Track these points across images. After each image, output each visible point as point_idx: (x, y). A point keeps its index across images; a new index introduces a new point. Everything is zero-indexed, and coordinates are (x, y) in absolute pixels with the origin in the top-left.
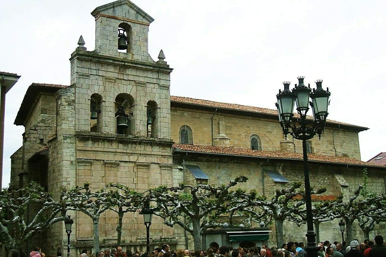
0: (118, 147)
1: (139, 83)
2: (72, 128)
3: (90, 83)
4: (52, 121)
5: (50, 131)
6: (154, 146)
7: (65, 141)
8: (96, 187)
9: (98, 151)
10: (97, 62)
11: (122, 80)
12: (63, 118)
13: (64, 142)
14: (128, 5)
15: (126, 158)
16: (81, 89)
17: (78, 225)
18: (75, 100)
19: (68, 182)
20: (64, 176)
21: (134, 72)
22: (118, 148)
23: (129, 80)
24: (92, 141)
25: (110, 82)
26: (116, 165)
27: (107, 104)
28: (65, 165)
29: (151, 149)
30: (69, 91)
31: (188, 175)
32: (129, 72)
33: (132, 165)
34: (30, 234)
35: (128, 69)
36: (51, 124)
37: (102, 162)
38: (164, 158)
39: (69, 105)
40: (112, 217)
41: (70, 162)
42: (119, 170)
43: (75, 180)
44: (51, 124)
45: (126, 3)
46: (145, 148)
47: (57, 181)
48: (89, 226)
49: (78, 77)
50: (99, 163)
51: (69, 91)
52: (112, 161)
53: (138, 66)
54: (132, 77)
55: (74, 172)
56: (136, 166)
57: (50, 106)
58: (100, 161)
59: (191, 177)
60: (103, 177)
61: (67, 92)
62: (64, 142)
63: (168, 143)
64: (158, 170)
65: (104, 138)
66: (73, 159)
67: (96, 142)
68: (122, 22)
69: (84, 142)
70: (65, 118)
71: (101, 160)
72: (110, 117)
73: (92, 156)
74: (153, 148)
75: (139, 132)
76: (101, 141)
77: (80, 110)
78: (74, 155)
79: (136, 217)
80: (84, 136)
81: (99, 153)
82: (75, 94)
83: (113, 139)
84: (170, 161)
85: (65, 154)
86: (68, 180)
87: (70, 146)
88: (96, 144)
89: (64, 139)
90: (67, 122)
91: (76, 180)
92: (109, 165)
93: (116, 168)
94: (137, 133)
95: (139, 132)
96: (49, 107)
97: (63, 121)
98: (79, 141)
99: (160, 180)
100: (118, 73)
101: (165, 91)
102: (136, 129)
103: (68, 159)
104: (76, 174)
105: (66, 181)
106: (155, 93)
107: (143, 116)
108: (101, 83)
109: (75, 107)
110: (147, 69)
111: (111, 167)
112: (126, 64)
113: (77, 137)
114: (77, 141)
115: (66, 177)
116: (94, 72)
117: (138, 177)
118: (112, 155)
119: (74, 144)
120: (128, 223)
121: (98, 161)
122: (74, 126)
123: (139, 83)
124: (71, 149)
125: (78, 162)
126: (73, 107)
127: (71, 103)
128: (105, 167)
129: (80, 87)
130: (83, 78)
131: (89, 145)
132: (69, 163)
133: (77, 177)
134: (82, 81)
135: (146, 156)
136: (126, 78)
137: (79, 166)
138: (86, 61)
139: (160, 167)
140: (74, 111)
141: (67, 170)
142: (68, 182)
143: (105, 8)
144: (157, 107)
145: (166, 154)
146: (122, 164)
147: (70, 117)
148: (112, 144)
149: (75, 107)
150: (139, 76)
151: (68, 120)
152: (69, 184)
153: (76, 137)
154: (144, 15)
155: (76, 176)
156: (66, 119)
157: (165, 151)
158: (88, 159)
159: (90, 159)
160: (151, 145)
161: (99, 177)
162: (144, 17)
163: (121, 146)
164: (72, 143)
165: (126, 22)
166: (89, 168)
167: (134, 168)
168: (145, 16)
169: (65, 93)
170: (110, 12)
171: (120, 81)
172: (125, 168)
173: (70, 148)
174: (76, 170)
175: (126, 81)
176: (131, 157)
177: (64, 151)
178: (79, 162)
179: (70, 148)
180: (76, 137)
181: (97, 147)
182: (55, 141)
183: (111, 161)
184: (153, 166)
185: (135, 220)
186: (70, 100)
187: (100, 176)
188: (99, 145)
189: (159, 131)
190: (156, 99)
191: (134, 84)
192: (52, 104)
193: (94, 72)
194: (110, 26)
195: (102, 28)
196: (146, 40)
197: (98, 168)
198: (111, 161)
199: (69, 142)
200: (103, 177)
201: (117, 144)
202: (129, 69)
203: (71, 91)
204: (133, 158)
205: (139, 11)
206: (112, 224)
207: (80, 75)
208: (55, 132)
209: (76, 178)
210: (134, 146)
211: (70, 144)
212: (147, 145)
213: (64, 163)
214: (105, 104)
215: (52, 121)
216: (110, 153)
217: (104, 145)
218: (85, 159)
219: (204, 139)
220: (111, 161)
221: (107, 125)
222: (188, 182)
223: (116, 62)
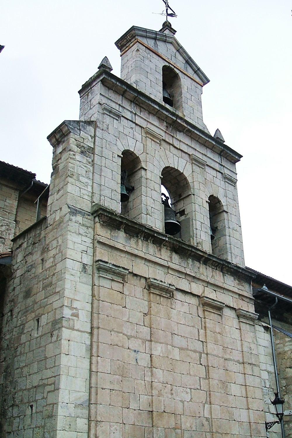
0: (171, 258)
1: (196, 160)
2: (86, 197)
3: (121, 129)
4: (7, 230)
5: (2, 245)
6: (227, 275)
7: (73, 218)
8: (133, 333)
9: (136, 256)
10: (133, 102)
11: (171, 146)
12: (69, 173)
13: (70, 220)
14: (174, 47)
15: (184, 284)
16: (106, 134)
17: (93, 424)
18: (93, 149)
19: (75, 311)
20: (67, 293)
21: (187, 140)
22: (172, 260)
23: (182, 151)
24: (125, 232)
25: (154, 141)
26: (167, 292)
27: (149, 175)
28: (71, 270)
29: (222, 277)
30: (85, 129)
31: (278, 342)
32: (180, 136)
33: (194, 301)
34: (181, 245)
35: (179, 133)
36: (4, 233)
37: (143, 281)
38: (243, 300)
39: (82, 152)
40: (164, 411)
41: (82, 266)
42: (173, 307)
43: (89, 307)
44: (4, 233)
45: (171, 43)
47: (40, 311)
48: (118, 428)
49: (101, 111)
50: (138, 281)
51: (85, 129)
52: (163, 284)
53: (195, 131)
54: (186, 146)
55: (86, 290)
56: (201, 306)
57: (6, 204)
58: (139, 278)
59: (289, 343)
60: (145, 314)
61: (80, 130)
62: (70, 220)
63: (247, 274)
64: (235, 322)
65: (148, 232)
66: (88, 260)
67: (133, 237)
69: (111, 231)
70: (74, 174)
71: (141, 277)
72: (154, 200)
73: (124, 262)
74: (225, 277)
76: (142, 239)
77: (103, 168)
78: (90, 251)
79: (207, 416)
80: (113, 217)
81: (138, 260)
82: (95, 139)
83: (164, 240)
84: (251, 309)
85: (70, 245)
86: (76, 305)
87: (82, 231)
88: (133, 241)
89: (71, 212)
90: (77, 183)
91: (92, 307)
92: (157, 292)
93: (169, 300)
94: (197, 243)
96: (5, 205)
97: (69, 179)
98: (102, 226)
99: (239, 343)
100: (165, 132)
101: (231, 188)
102: (195, 235)
103: (78, 257)
104: (93, 296)
105: (72, 308)
107: (205, 217)
108: (139, 137)
109: (93, 161)
110: (206, 144)
111: (160, 295)
112: (179, 121)
113: (98, 216)
114: (98, 225)
115: (72, 296)
116: (129, 115)
117: (205, 327)
118: (160, 272)
119: (90, 230)
120: (194, 428)
121: (135, 278)
122: (90, 195)
123: (196, 160)
124: (85, 239)
125: (99, 269)
126: (90, 160)
127: (88, 151)
128: (150, 293)
129: (104, 129)
130: (109, 116)
131: (120, 239)
132: (78, 267)
133: (95, 301)
134: (108, 120)
136: (176, 143)
137: (101, 279)
138: (116, 92)
139: (238, 316)
140: (91, 168)
141: (74, 283)
142: (75, 311)
143: (144, 34)
144: (221, 211)
145: (245, 294)
146: (179, 296)
147: (83, 176)
148: (160, 250)
149: (93, 161)
150: (196, 150)
151: (78, 180)
152: (77, 316)
153: (95, 217)
154: (197, 70)
155: (93, 300)
156: (75, 177)
158: (119, 267)
159: (124, 268)
160: (222, 271)
161: (138, 314)
162: (195, 72)
163: (176, 257)
164: (88, 227)
166: (117, 286)
167: (199, 307)
168: (197, 71)
169: (76, 129)
171: (167, 146)
172: (183, 305)
173: (81, 235)
174: (93, 285)
175: (176, 150)
176: (193, 285)
177: (69, 237)
178: (101, 267)
179: (81, 235)
180: (95, 217)
181: (135, 247)
182: (35, 230)
183: (161, 283)
184: (227, 312)
185: (206, 423)
186: (85, 146)
187: (139, 311)
188: (138, 246)
189: (229, 250)
190: (220, 195)
191: (188, 159)
192: (11, 202)
193: (129, 115)
194: (150, 61)
195: (139, 59)
196: (200, 103)
197: (135, 290)
198: (161, 283)
199: (81, 221)
200: (145, 314)
201: (169, 253)
202: (181, 133)
203: (87, 131)
204: (197, 288)
205: (189, 60)
206: (165, 429)
207: (105, 109)
208: (9, 248)
209: (92, 304)
210: (197, 264)
211: (84, 228)
212: (217, 269)
213: (69, 263)
214: (146, 175)
215: (7, 230)
216: (158, 267)
217: (147, 247)
218: (113, 265)
219: (136, 382)
220: (161, 281)
221: (150, 212)
222: (280, 353)
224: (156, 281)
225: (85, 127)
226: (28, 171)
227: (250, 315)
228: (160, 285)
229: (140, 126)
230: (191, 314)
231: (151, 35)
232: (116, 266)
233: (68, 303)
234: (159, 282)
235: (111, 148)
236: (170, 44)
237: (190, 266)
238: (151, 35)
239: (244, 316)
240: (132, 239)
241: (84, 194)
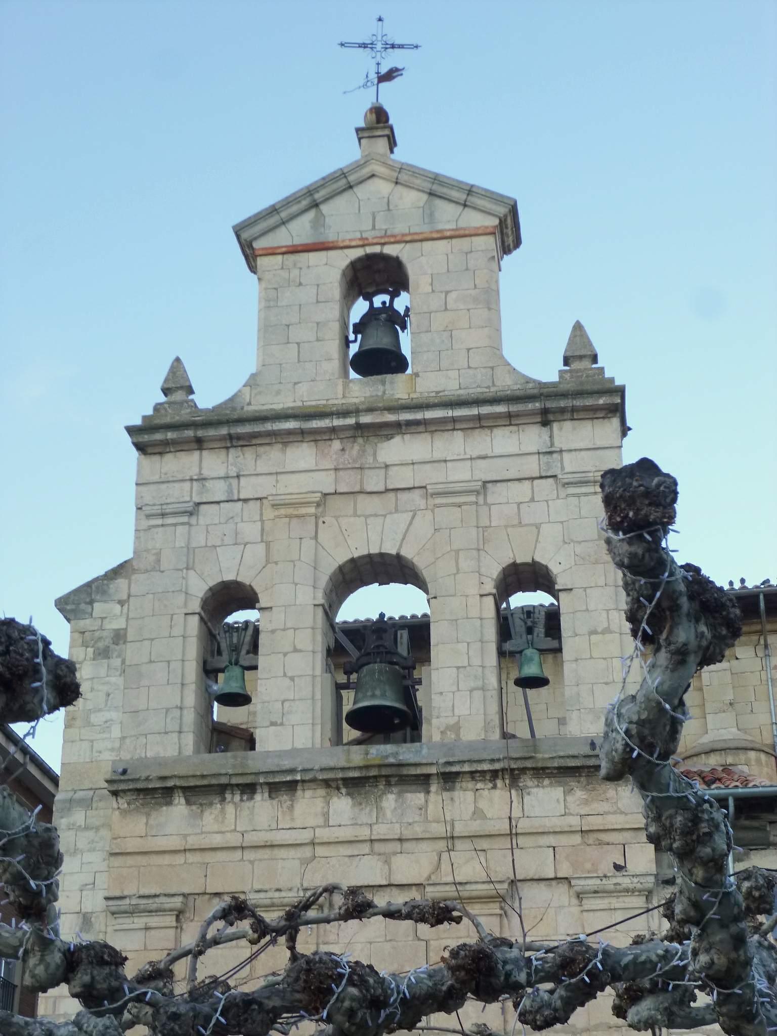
38: (601, 843)
46: (483, 804)
68: (358, 253)
69: (148, 815)
72: (292, 679)
75: (456, 728)
95: (456, 728)
106: (538, 527)
135: (484, 844)
157: (604, 807)
165: (377, 249)
170: (300, 230)
198: (277, 894)
210: (416, 798)
223: (315, 424)
224: (262, 895)
225: (105, 587)
226: (362, 619)
227: (615, 884)
228: (275, 900)
229: (257, 499)
230: (390, 940)
231: (335, 186)
232: (148, 897)
233: (46, 1009)
234: (270, 895)
235: (166, 606)
236: (371, 181)
237: (389, 814)
238: (335, 186)
239: (596, 892)
240: (207, 814)
241: (100, 752)
